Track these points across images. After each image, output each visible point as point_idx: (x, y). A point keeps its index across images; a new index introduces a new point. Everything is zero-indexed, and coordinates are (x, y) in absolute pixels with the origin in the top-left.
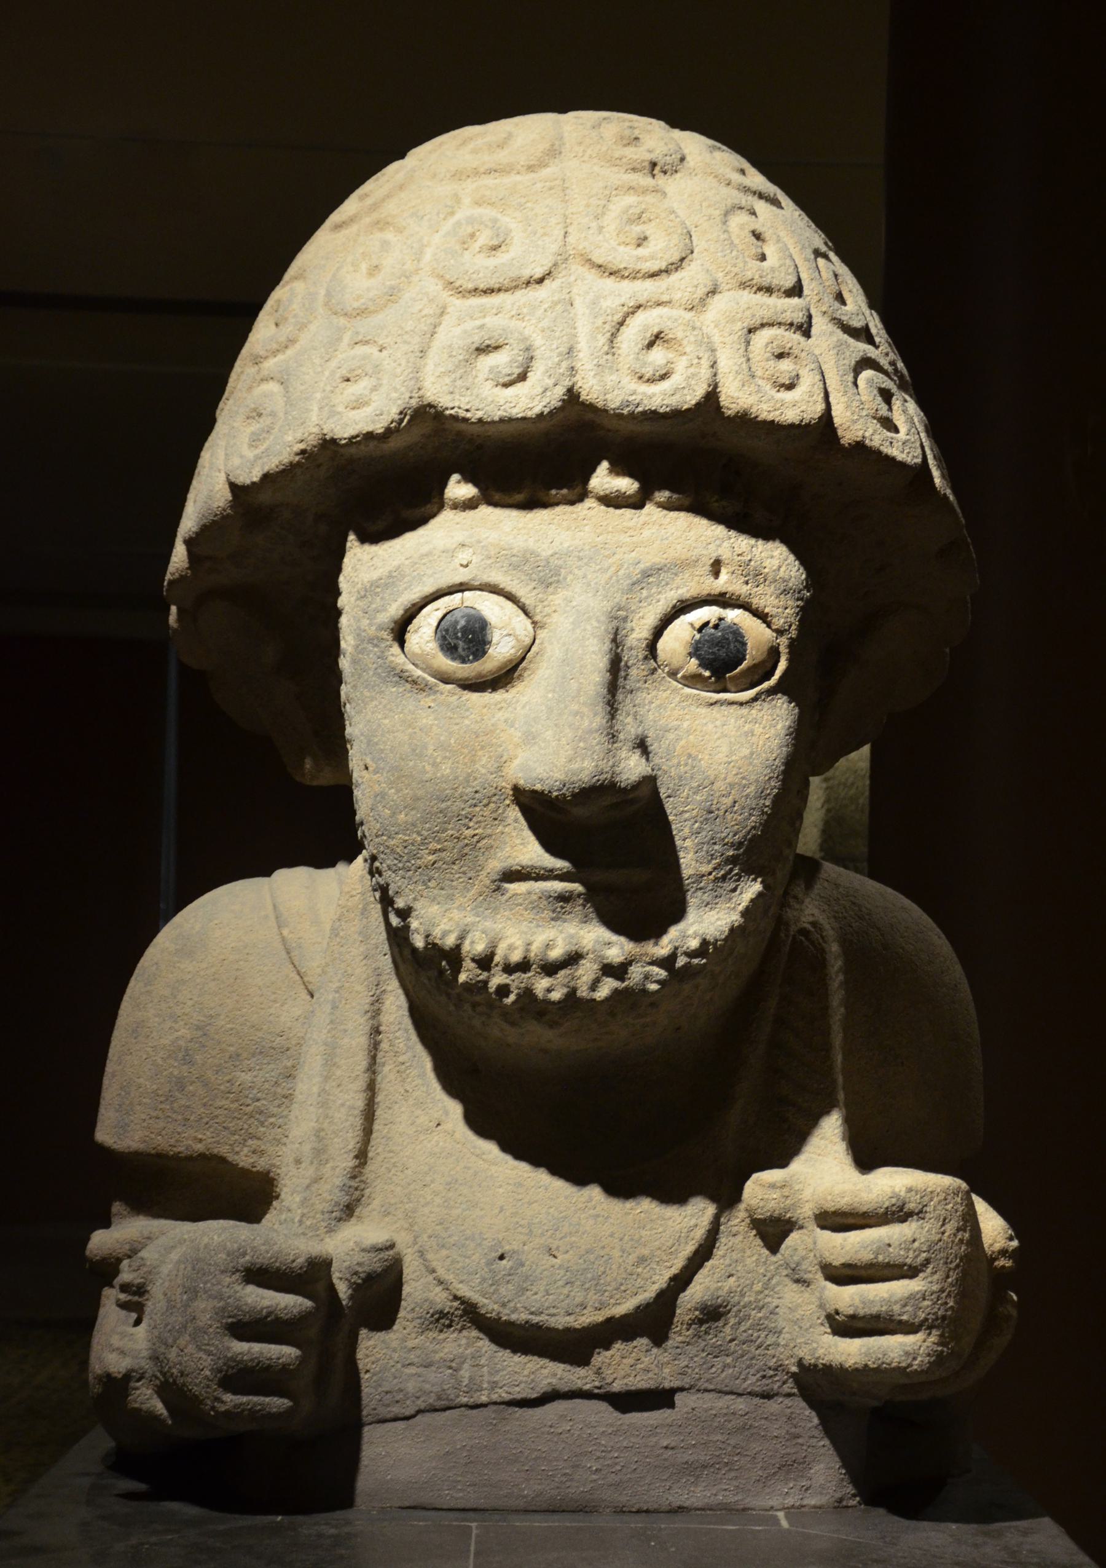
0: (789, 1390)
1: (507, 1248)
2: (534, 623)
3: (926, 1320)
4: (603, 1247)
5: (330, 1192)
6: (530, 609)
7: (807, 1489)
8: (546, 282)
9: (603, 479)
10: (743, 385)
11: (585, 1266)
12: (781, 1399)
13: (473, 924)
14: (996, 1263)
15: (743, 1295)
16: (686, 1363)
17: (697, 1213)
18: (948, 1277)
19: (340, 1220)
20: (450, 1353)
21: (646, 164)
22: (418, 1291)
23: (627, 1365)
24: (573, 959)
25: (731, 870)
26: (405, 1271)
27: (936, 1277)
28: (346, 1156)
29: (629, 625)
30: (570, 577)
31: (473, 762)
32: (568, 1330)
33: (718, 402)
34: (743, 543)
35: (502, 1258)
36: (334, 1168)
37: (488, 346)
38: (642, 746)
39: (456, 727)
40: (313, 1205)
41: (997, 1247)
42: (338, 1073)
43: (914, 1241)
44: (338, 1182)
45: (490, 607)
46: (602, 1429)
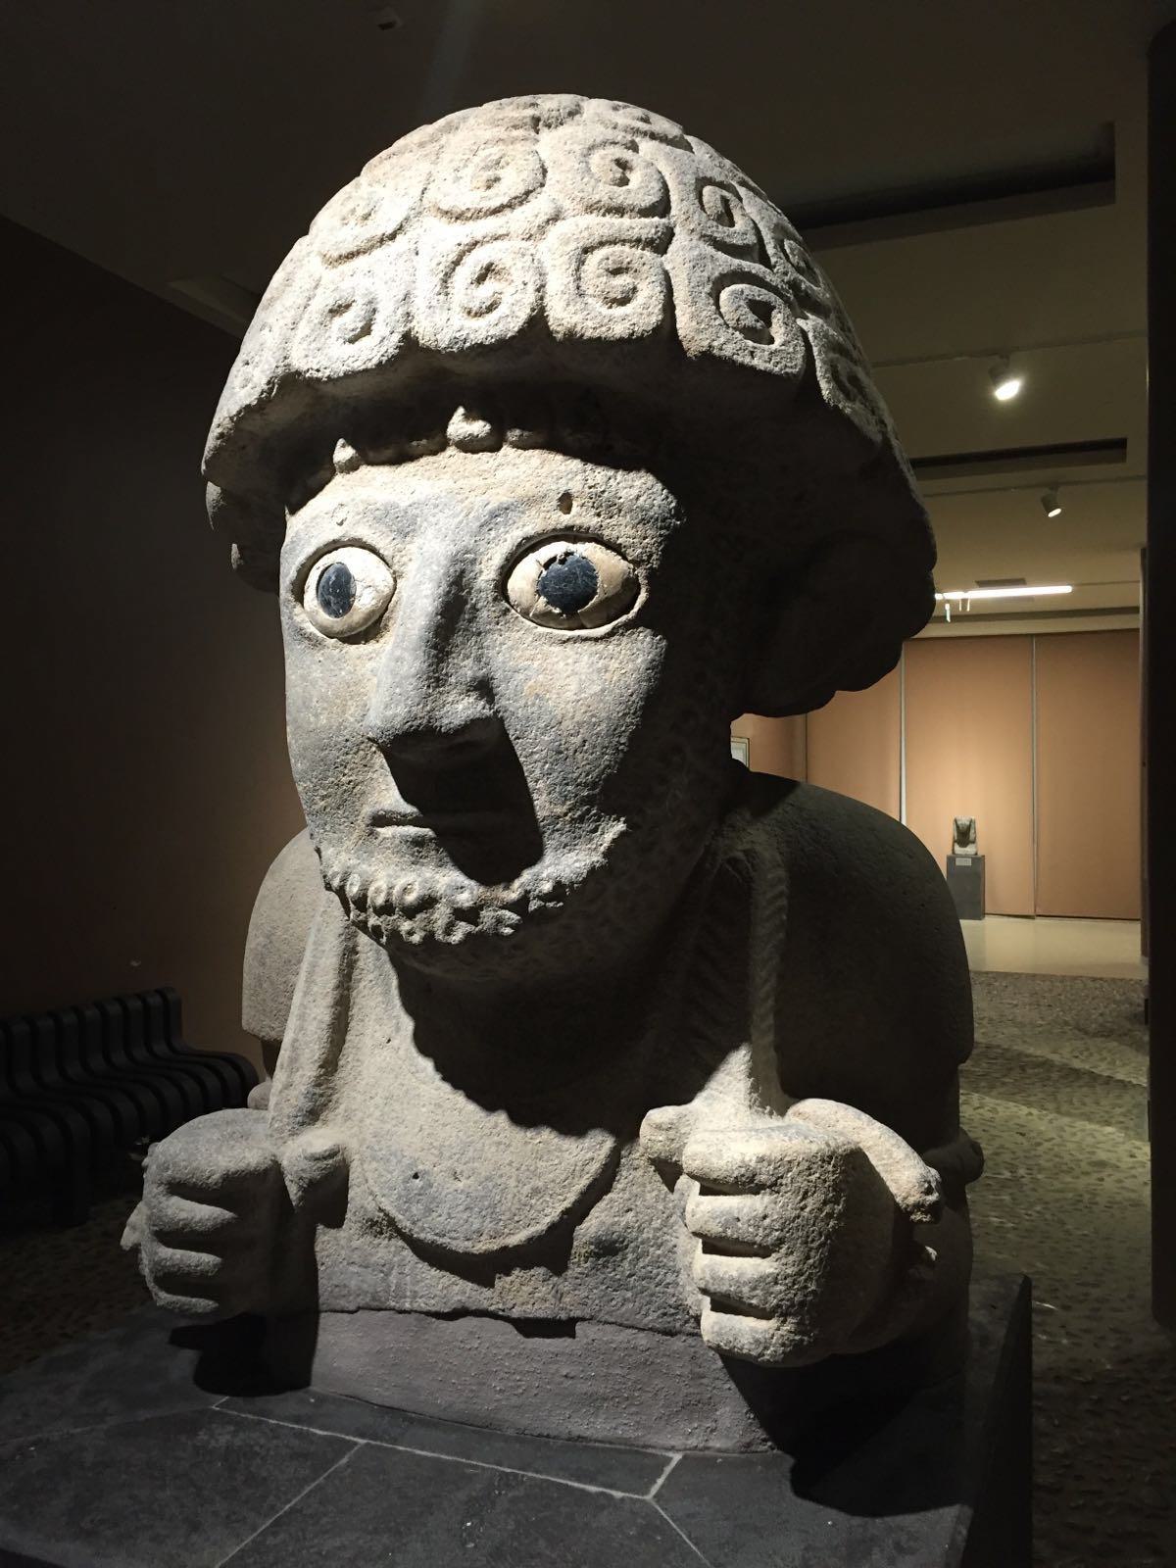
0: (692, 1330)
1: (421, 1167)
2: (396, 577)
3: (778, 1306)
4: (501, 1176)
5: (297, 1098)
6: (388, 559)
7: (712, 1431)
8: (399, 237)
9: (460, 426)
10: (568, 305)
11: (483, 1194)
12: (684, 1338)
13: (354, 867)
14: (913, 1217)
15: (640, 1230)
16: (586, 1294)
17: (596, 1147)
18: (808, 1258)
19: (302, 1124)
20: (382, 1258)
21: (528, 120)
22: (361, 1198)
23: (527, 1292)
24: (428, 903)
25: (588, 811)
26: (351, 1177)
27: (791, 1258)
28: (312, 1065)
29: (477, 568)
30: (425, 524)
31: (344, 712)
32: (467, 1254)
33: (548, 327)
34: (599, 475)
35: (416, 1176)
36: (302, 1076)
37: (340, 306)
38: (484, 688)
39: (334, 679)
40: (281, 1108)
41: (911, 1200)
42: (315, 989)
43: (765, 1217)
44: (303, 1089)
45: (354, 560)
46: (507, 1351)
